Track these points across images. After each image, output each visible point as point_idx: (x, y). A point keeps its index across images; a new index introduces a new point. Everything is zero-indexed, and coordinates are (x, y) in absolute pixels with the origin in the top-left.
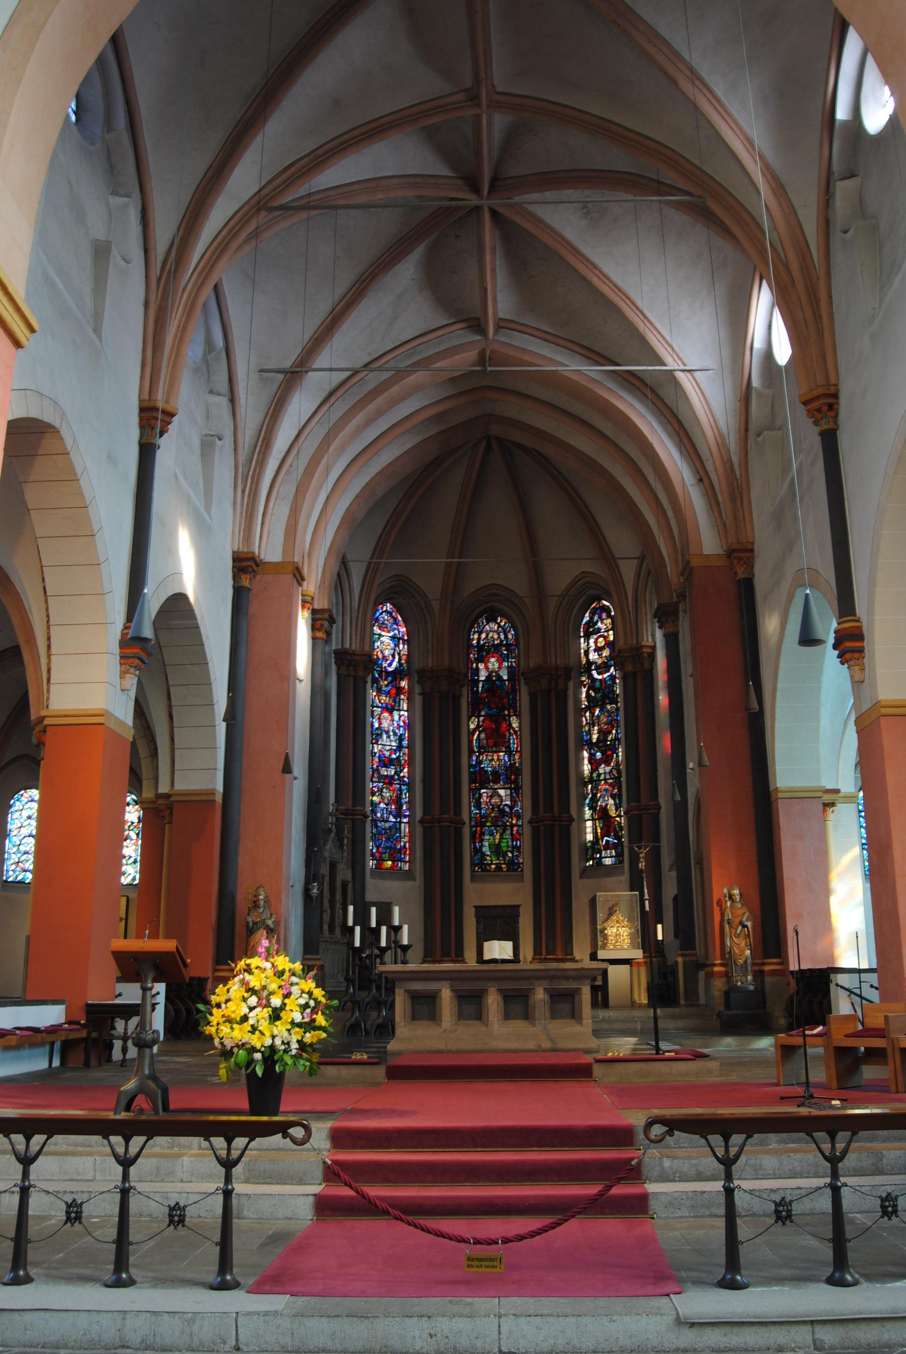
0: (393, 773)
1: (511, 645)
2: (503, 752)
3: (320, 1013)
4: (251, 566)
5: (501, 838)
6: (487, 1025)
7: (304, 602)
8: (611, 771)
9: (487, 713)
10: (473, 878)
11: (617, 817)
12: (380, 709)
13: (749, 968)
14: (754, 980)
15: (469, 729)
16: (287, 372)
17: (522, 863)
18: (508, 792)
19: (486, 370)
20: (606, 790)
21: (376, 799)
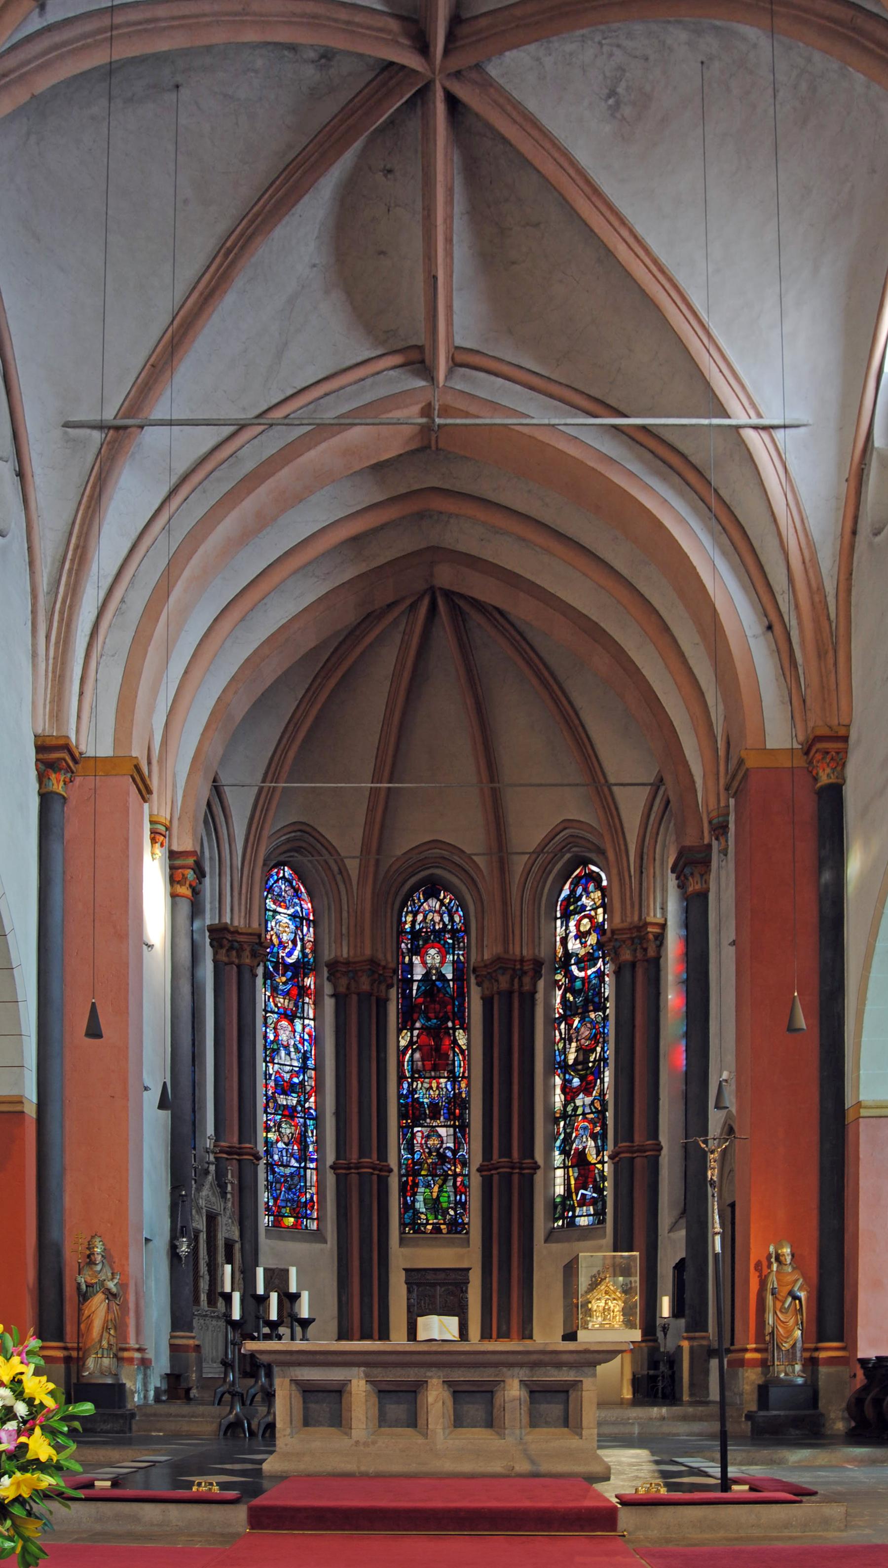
0: (295, 1102)
1: (458, 931)
2: (444, 1078)
3: (38, 1430)
4: (65, 760)
5: (441, 1191)
6: (425, 1435)
7: (153, 832)
8: (592, 1103)
9: (423, 1025)
10: (402, 1242)
11: (599, 1162)
12: (276, 1016)
13: (798, 1354)
14: (803, 1371)
15: (398, 1046)
16: (109, 428)
17: (468, 1224)
18: (451, 1130)
19: (434, 421)
20: (585, 1128)
21: (272, 1136)
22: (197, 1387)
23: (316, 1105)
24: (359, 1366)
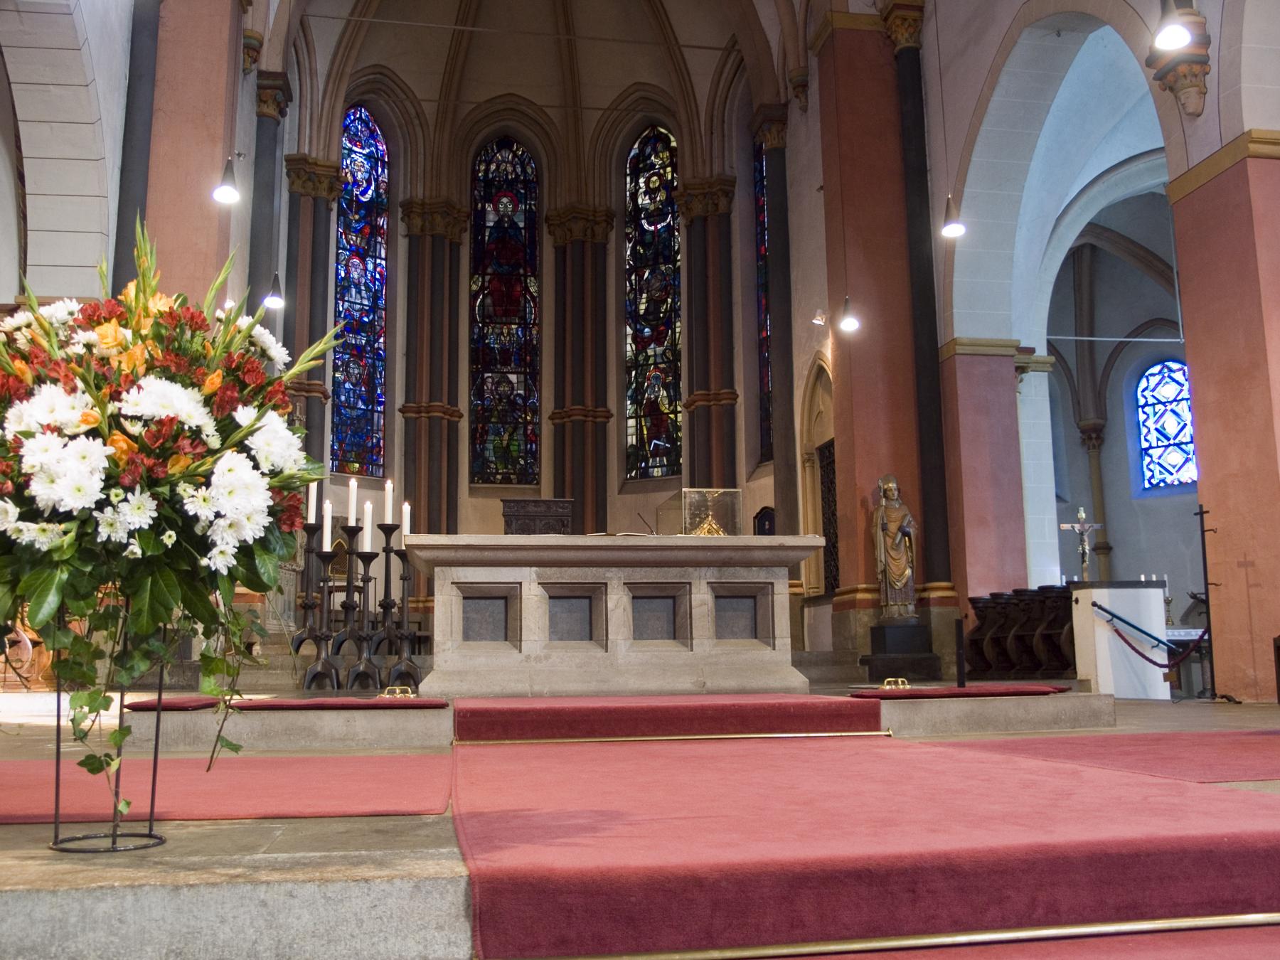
2: (515, 324)
8: (664, 353)
11: (671, 413)
18: (522, 377)
20: (657, 378)
22: (260, 644)
23: (385, 346)
24: (531, 566)
